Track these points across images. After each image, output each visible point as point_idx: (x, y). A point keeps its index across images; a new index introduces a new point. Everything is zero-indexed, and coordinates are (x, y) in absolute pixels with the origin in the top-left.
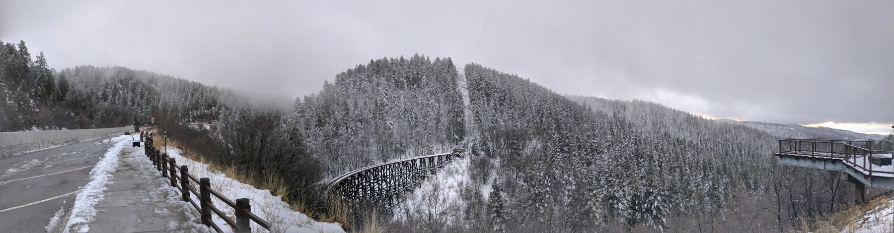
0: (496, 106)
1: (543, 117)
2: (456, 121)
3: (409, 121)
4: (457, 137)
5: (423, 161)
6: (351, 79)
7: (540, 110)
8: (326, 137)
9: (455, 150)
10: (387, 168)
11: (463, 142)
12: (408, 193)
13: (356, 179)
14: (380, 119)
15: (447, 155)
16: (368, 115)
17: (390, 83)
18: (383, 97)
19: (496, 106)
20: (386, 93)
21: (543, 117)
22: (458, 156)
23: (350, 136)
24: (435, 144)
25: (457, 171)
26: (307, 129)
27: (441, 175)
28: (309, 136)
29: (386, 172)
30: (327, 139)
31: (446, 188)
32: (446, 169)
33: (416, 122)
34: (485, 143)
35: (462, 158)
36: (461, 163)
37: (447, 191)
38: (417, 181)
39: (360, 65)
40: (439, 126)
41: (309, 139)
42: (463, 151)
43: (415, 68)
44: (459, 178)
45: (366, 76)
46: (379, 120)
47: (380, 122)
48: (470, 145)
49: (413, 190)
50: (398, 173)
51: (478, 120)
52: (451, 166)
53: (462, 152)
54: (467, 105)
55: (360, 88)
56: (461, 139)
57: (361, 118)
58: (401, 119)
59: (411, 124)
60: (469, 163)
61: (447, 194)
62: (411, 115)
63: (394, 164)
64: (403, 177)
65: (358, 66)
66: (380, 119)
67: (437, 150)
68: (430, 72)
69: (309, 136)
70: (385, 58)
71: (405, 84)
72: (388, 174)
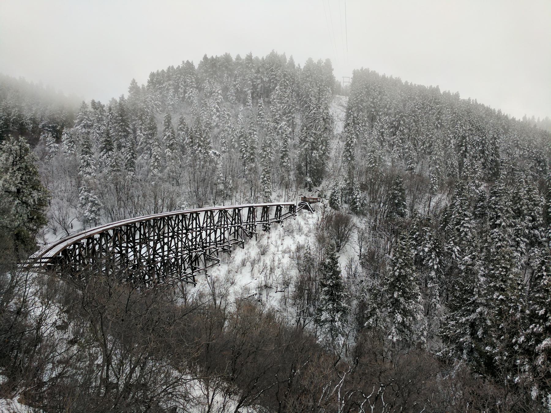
0: (383, 136)
1: (465, 157)
2: (311, 157)
3: (241, 151)
4: (309, 180)
5: (252, 210)
6: (171, 82)
7: (462, 146)
8: (115, 167)
9: (304, 199)
10: (193, 217)
11: (320, 188)
12: (226, 254)
13: (138, 229)
14: (199, 146)
15: (291, 205)
16: (184, 140)
17: (229, 93)
18: (212, 113)
19: (383, 136)
20: (217, 108)
21: (465, 157)
22: (306, 208)
23: (152, 168)
24: (277, 188)
25: (300, 230)
26: (86, 153)
27: (275, 233)
28: (88, 165)
29: (192, 223)
30: (115, 171)
31: (280, 252)
32: (284, 225)
33: (252, 154)
34: (351, 192)
35: (312, 211)
36: (309, 218)
37: (280, 256)
38: (240, 240)
39: (188, 61)
40: (284, 162)
41: (88, 170)
42: (315, 201)
43: (267, 74)
44: (301, 239)
45: (194, 80)
46: (198, 147)
47: (200, 151)
48: (329, 194)
49: (231, 251)
50: (168, 233)
51: (349, 156)
52: (293, 222)
53: (313, 202)
54: (340, 132)
55: (184, 97)
56: (317, 182)
57: (171, 142)
58: (234, 148)
59: (245, 156)
60: (320, 220)
61: (279, 260)
62: (245, 143)
63: (177, 216)
64: (176, 239)
65: (185, 62)
66: (199, 146)
67: (278, 196)
68: (287, 80)
69: (88, 165)
70: (113, 99)
71: (249, 97)
72: (194, 226)
